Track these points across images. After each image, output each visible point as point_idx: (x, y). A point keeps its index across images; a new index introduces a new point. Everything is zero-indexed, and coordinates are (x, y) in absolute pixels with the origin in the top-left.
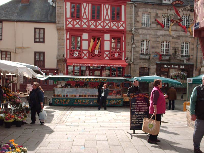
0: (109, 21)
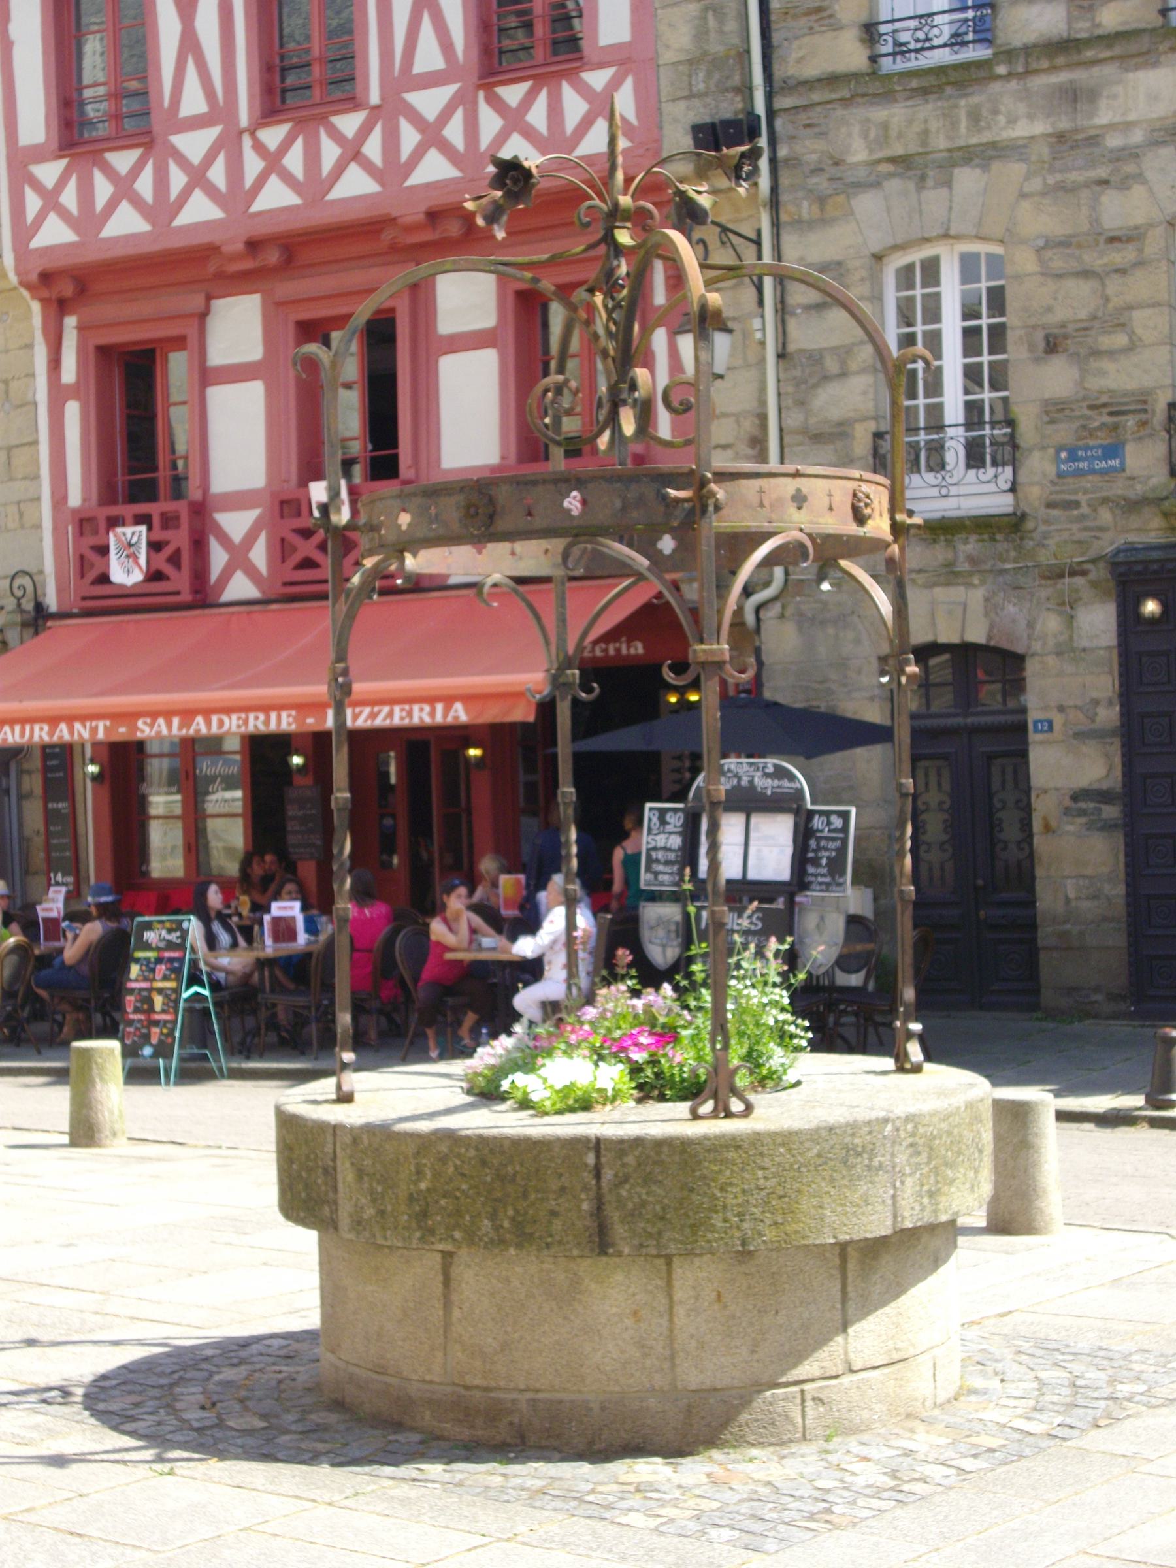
0: (446, 92)
